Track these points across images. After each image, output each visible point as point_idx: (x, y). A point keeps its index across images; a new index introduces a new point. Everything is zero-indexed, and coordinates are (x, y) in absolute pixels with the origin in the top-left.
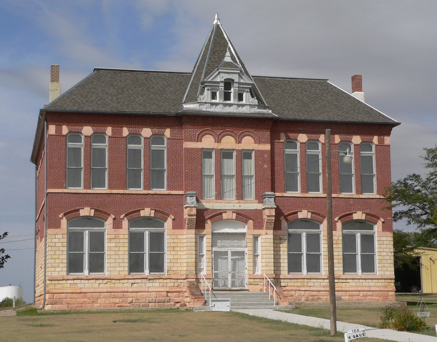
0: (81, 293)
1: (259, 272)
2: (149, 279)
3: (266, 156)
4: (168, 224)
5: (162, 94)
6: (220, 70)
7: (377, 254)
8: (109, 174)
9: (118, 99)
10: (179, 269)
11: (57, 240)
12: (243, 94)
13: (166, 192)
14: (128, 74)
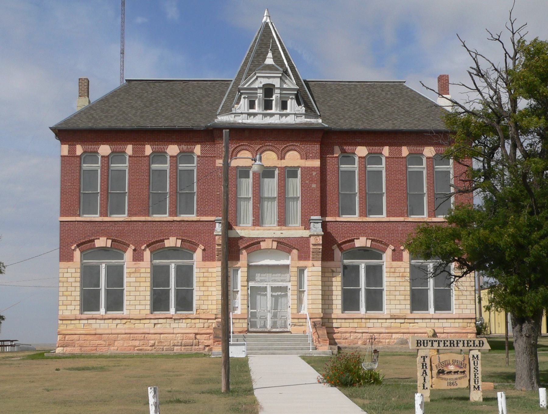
0: (95, 334)
2: (175, 319)
3: (314, 174)
4: (198, 254)
5: (196, 106)
6: (257, 75)
8: (129, 199)
10: (210, 307)
11: (69, 275)
12: (255, 101)
13: (101, 219)
14: (163, 84)
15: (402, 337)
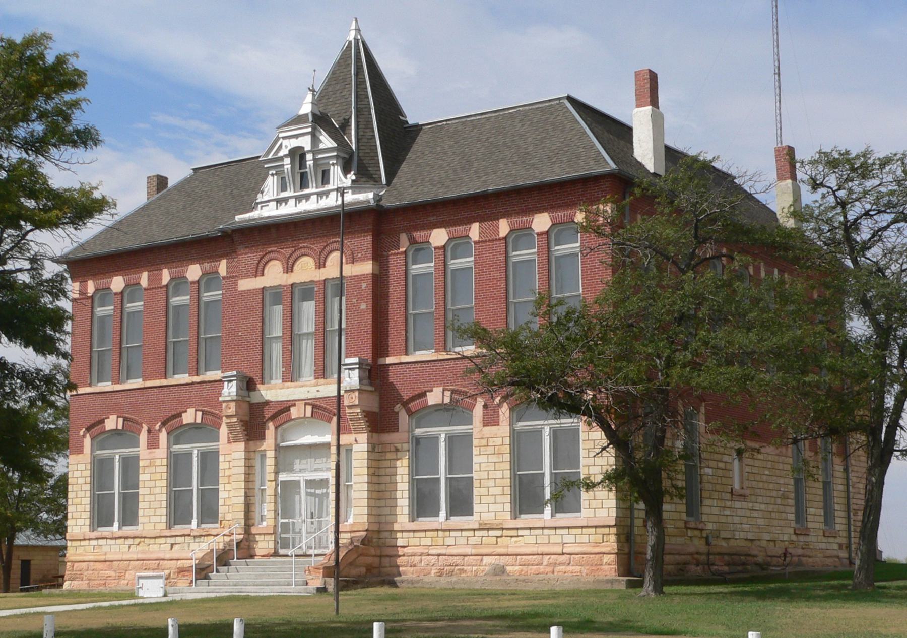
0: (105, 561)
2: (194, 537)
3: (364, 285)
15: (497, 562)
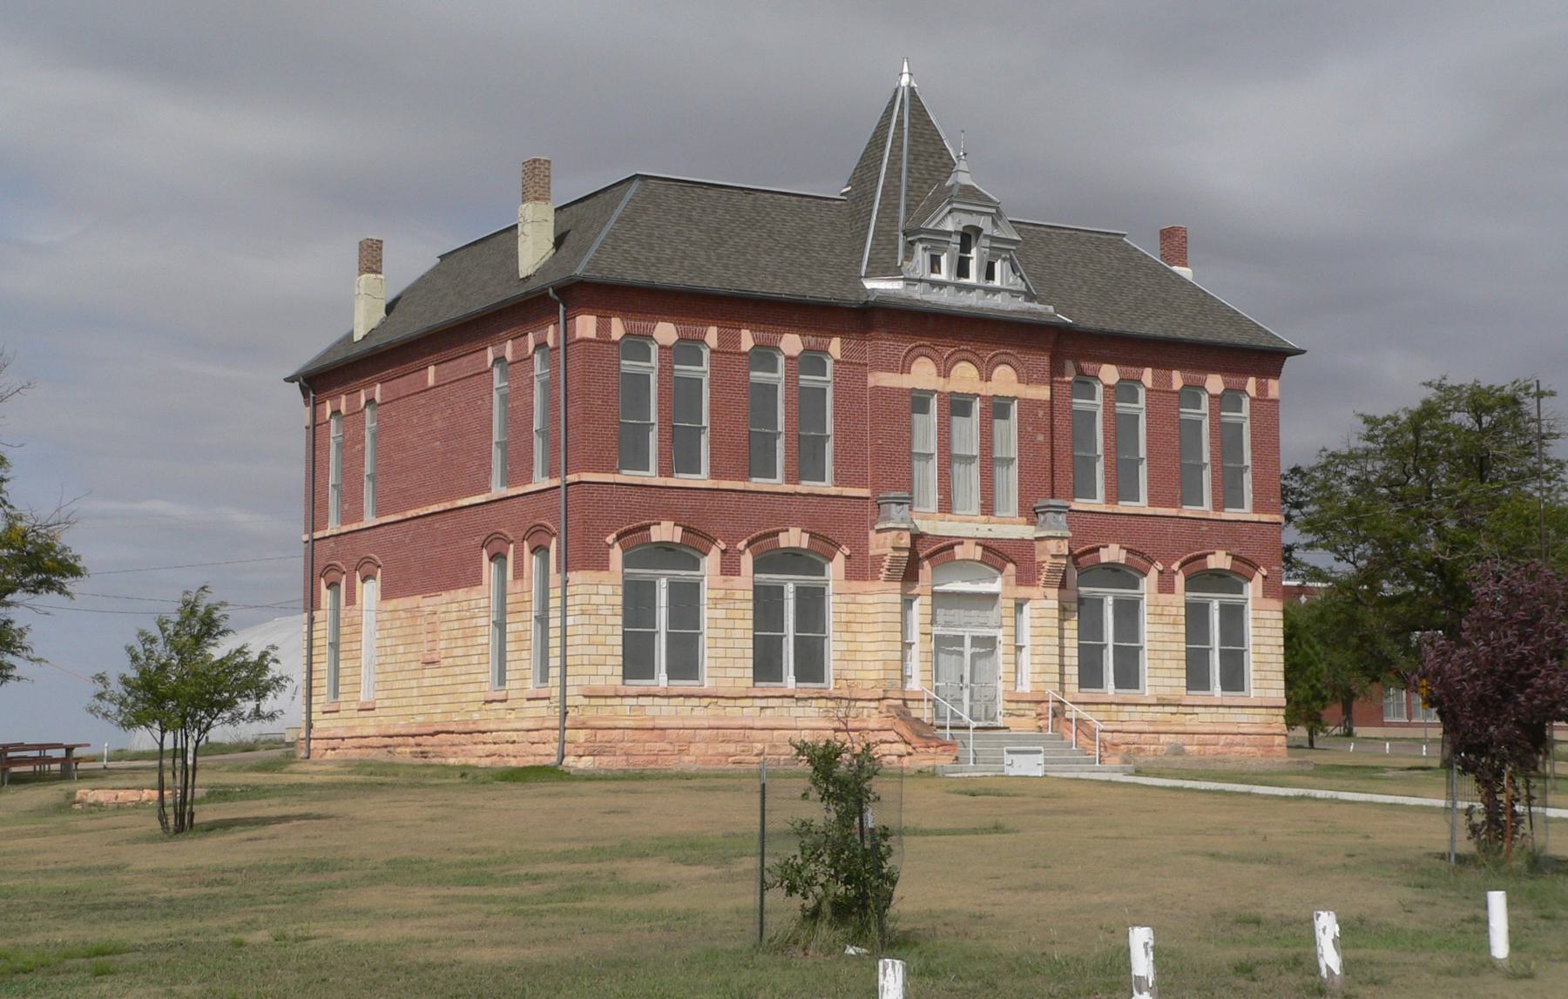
1: (1025, 688)
3: (1041, 413)
4: (835, 568)
7: (1251, 649)
8: (712, 442)
9: (720, 257)
11: (601, 600)
